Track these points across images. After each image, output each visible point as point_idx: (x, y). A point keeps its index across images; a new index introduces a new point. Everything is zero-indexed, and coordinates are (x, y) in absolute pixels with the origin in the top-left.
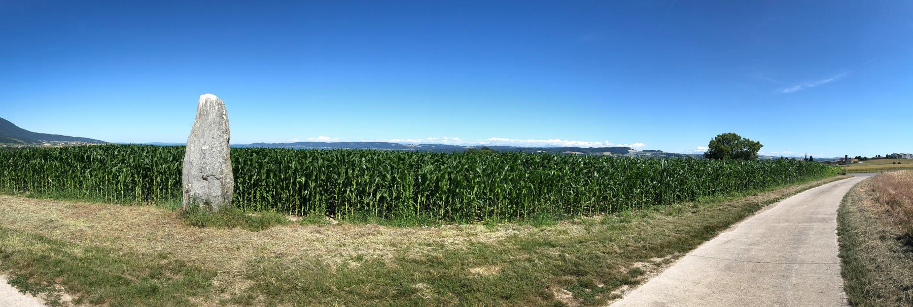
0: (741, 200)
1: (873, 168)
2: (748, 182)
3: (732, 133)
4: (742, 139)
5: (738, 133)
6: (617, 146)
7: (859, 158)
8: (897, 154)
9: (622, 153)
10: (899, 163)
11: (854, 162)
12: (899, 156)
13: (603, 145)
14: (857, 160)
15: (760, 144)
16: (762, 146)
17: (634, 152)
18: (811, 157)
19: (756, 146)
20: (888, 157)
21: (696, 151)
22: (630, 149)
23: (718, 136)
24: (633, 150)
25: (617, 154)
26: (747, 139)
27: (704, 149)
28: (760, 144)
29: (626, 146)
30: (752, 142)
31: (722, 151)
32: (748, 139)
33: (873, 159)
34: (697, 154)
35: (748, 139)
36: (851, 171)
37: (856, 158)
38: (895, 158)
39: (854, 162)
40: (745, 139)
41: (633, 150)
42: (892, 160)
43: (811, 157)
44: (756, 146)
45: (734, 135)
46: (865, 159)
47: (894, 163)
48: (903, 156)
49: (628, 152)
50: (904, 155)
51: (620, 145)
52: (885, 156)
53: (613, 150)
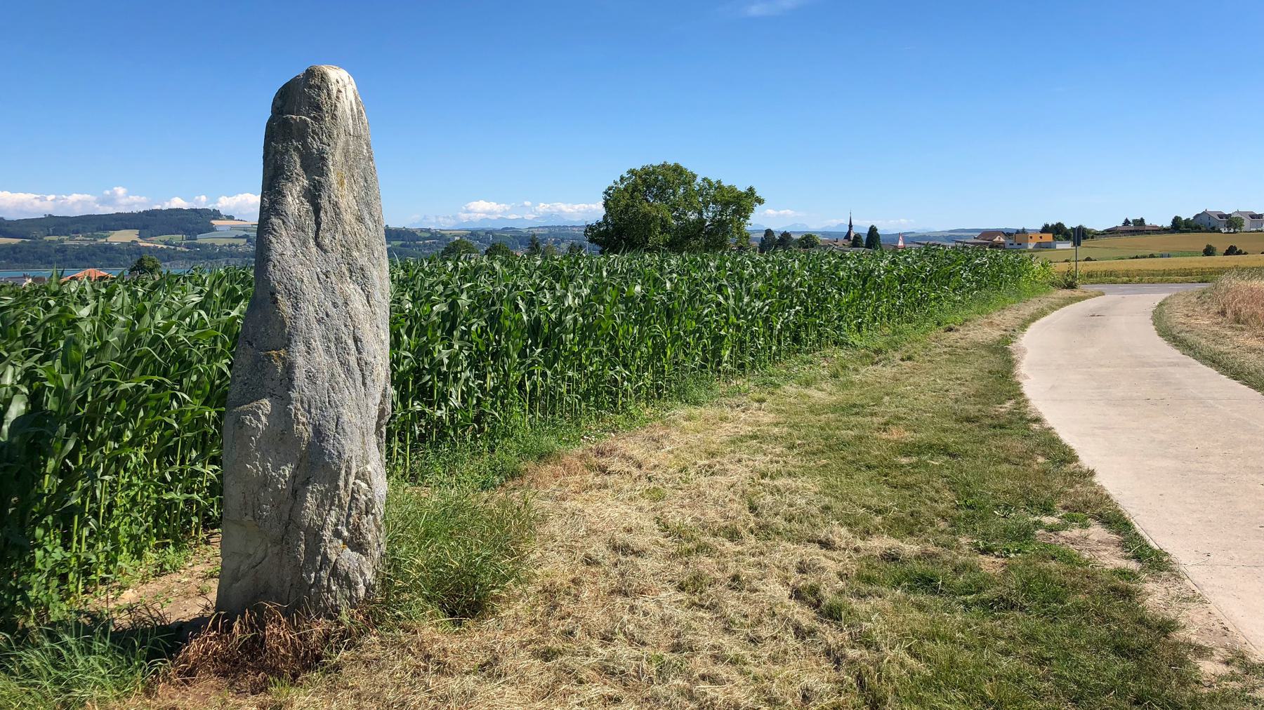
0: (1097, 288)
1: (1151, 267)
2: (635, 350)
3: (671, 163)
4: (699, 180)
5: (689, 165)
6: (166, 206)
7: (1057, 231)
8: (1221, 216)
9: (186, 232)
10: (1231, 251)
11: (1040, 246)
12: (1232, 222)
13: (103, 202)
14: (1048, 237)
15: (757, 195)
16: (760, 201)
17: (232, 228)
18: (873, 230)
19: (742, 203)
20: (1178, 226)
21: (464, 217)
22: (216, 214)
23: (632, 172)
24: (231, 218)
25: (166, 237)
26: (714, 180)
27: (592, 210)
28: (757, 195)
29: (202, 202)
30: (732, 189)
31: (647, 220)
32: (719, 182)
33: (1111, 232)
34: (471, 227)
35: (719, 182)
36: (1110, 278)
37: (1046, 229)
38: (1214, 230)
39: (1040, 246)
40: (710, 183)
41: (231, 218)
42: (1200, 240)
43: (873, 230)
44: (742, 203)
45: (678, 170)
46: (1079, 235)
47: (1209, 251)
48: (1247, 224)
49: (211, 229)
50: (1253, 216)
51: (178, 203)
52: (1167, 223)
53: (148, 221)
